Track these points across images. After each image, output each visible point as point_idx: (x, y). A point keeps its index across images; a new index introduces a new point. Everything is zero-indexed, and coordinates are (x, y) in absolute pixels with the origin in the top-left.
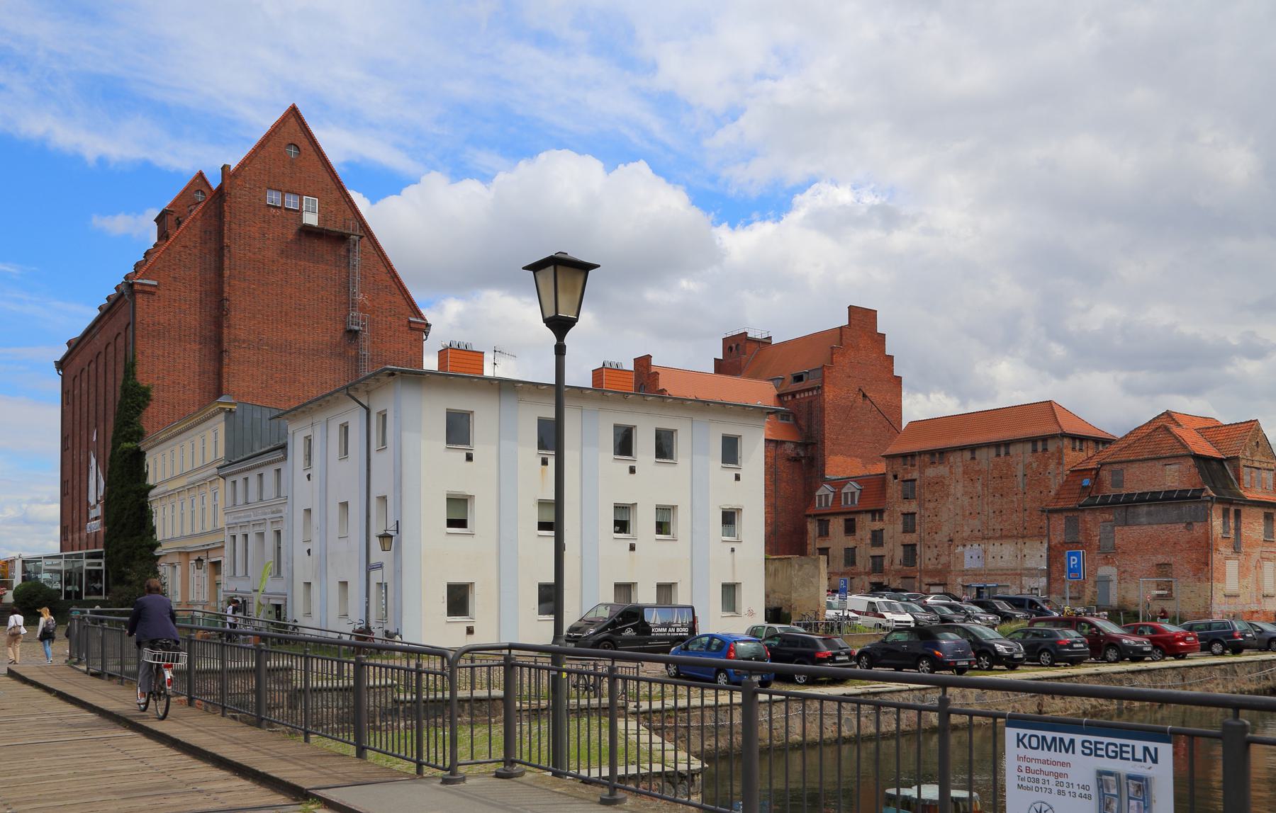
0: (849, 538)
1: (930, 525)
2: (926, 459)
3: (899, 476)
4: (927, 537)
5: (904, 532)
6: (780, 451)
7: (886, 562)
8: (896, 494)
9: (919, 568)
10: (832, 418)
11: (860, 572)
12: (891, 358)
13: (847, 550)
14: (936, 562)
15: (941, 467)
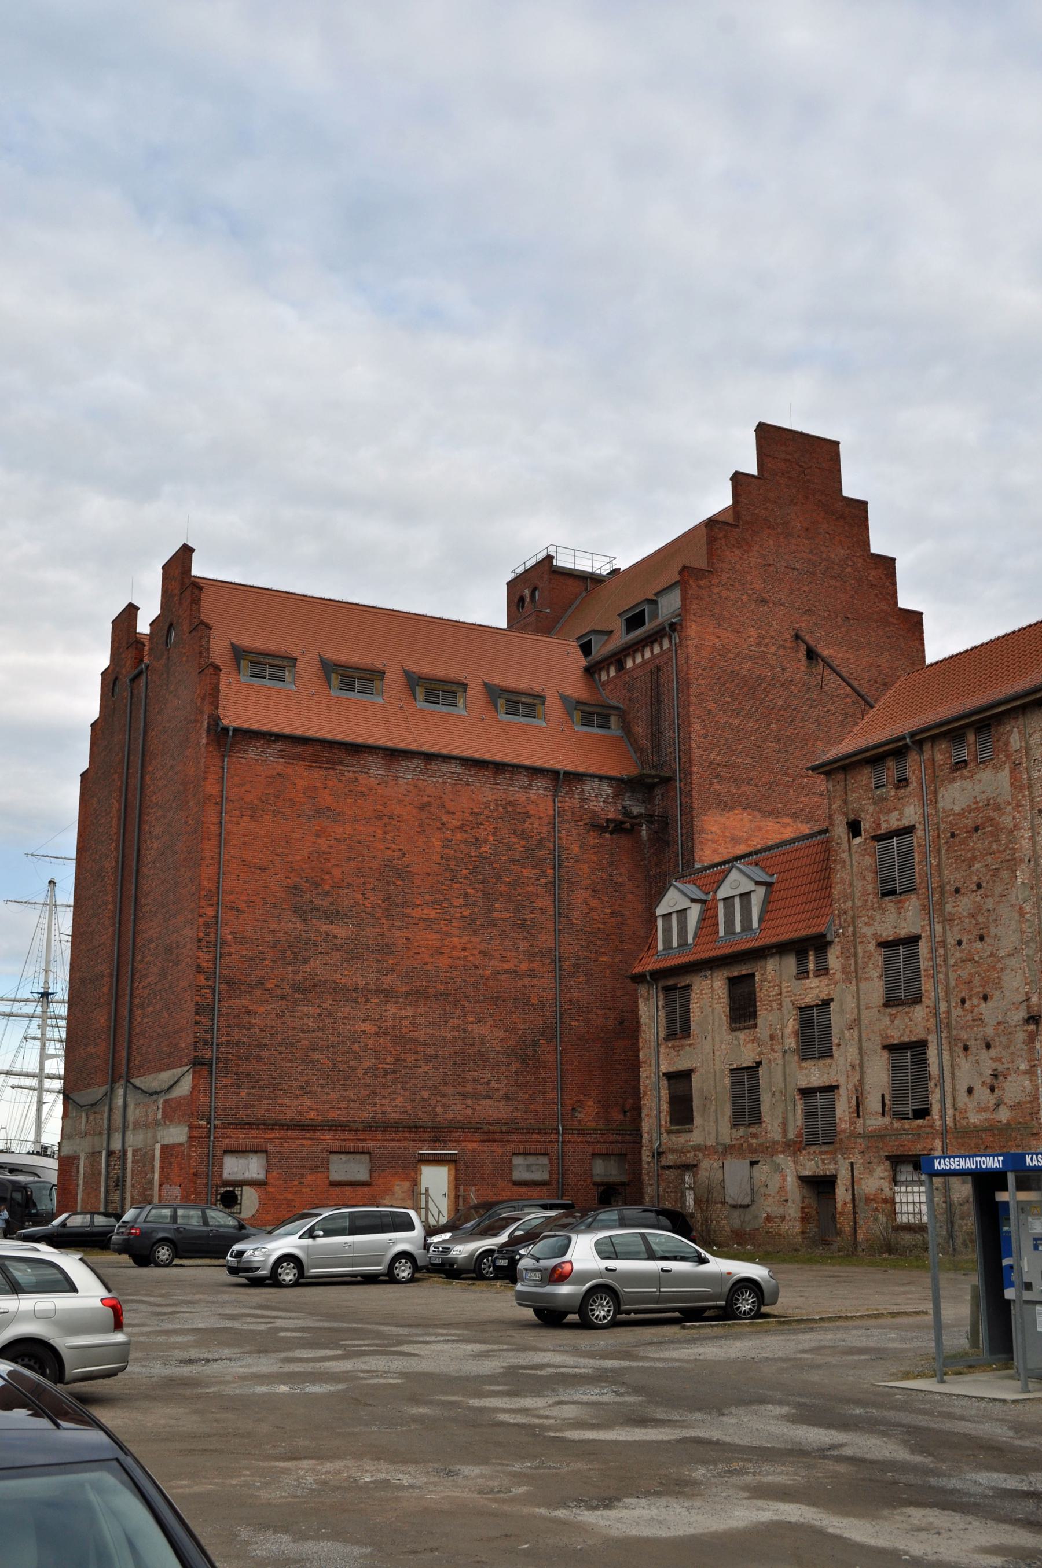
0: (742, 1035)
1: (965, 974)
2: (939, 757)
3: (865, 826)
4: (957, 1012)
5: (886, 1005)
6: (569, 802)
7: (843, 1108)
8: (859, 884)
9: (938, 1123)
10: (713, 706)
11: (775, 1143)
12: (888, 563)
13: (736, 1072)
14: (991, 1099)
15: (986, 775)
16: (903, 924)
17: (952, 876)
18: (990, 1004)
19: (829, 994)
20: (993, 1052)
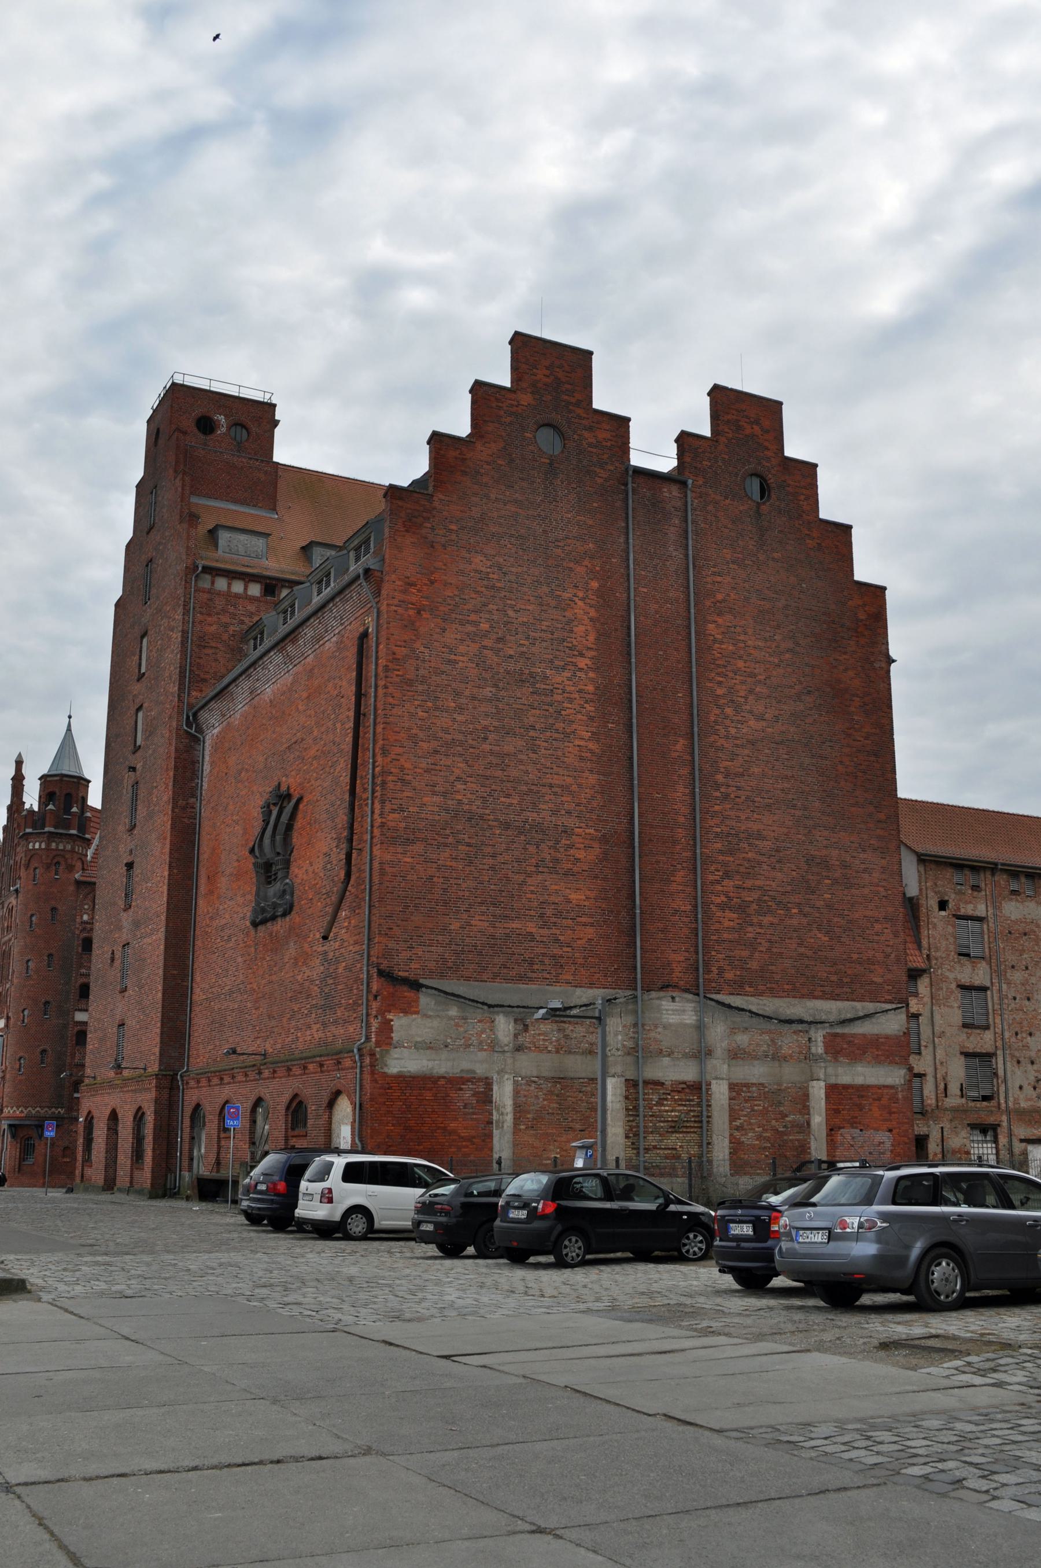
1: (1018, 1018)
4: (1013, 1039)
5: (965, 1026)
16: (976, 978)
17: (1011, 958)
18: (1033, 1038)
19: (918, 1010)
20: (1035, 1067)
